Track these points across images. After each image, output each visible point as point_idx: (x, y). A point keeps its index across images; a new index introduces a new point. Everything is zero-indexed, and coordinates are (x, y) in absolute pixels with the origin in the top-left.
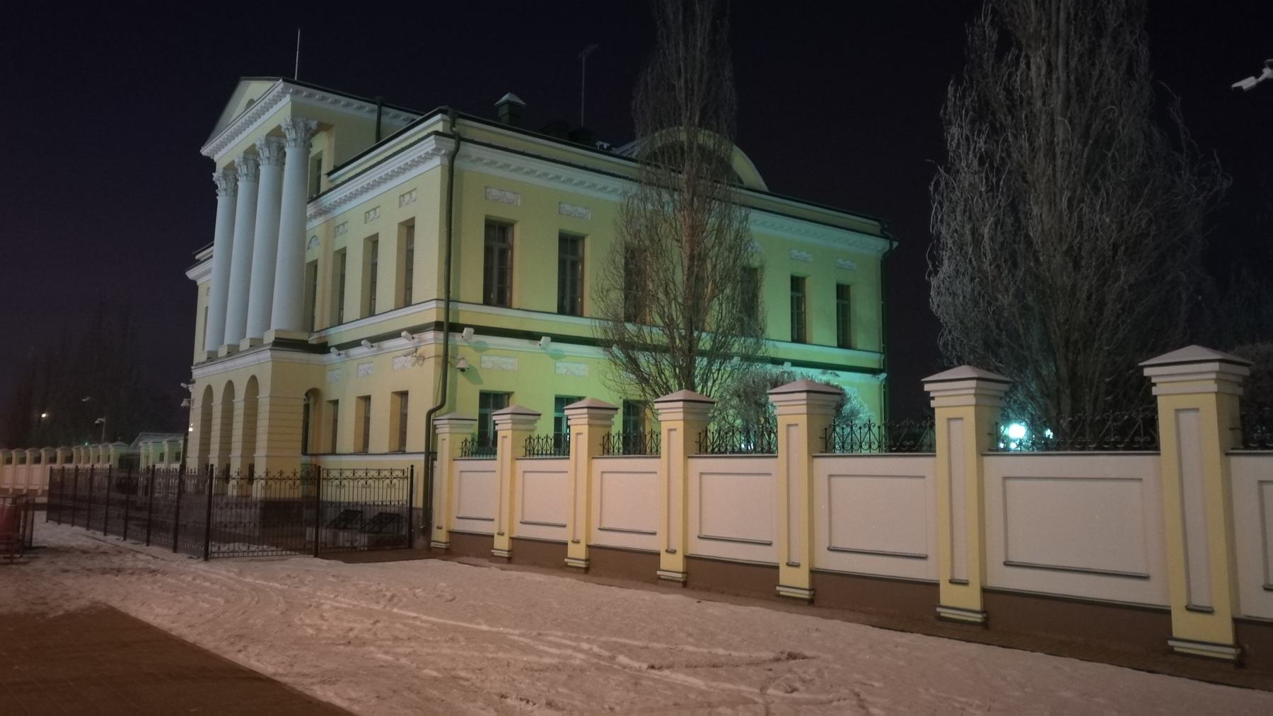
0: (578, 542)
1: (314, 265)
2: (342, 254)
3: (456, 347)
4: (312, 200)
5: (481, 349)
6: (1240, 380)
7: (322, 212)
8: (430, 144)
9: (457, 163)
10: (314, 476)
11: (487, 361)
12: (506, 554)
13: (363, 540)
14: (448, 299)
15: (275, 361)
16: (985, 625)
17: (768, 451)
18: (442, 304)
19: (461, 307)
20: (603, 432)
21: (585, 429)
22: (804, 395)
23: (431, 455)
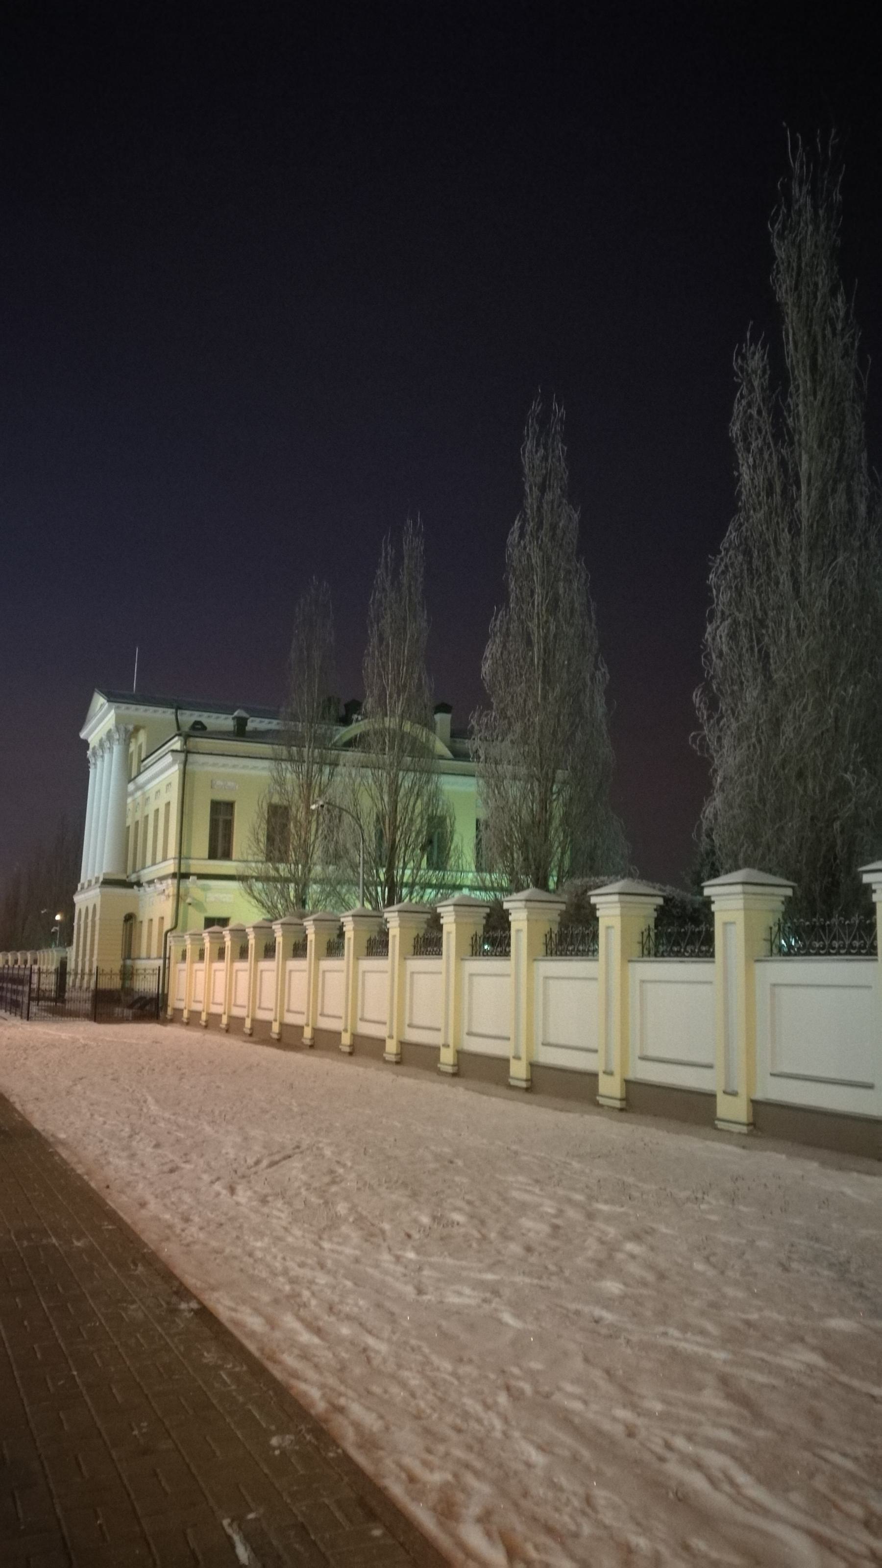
0: (734, 1094)
1: (129, 827)
2: (147, 817)
3: (187, 890)
4: (131, 780)
5: (205, 889)
6: (783, 899)
7: (139, 788)
8: (169, 758)
9: (188, 767)
10: (127, 974)
11: (211, 897)
12: (524, 1084)
13: (128, 1012)
14: (180, 857)
15: (103, 895)
16: (279, 1040)
17: (506, 954)
18: (177, 861)
19: (191, 862)
20: (198, 948)
21: (739, 917)
22: (616, 898)
23: (166, 958)
